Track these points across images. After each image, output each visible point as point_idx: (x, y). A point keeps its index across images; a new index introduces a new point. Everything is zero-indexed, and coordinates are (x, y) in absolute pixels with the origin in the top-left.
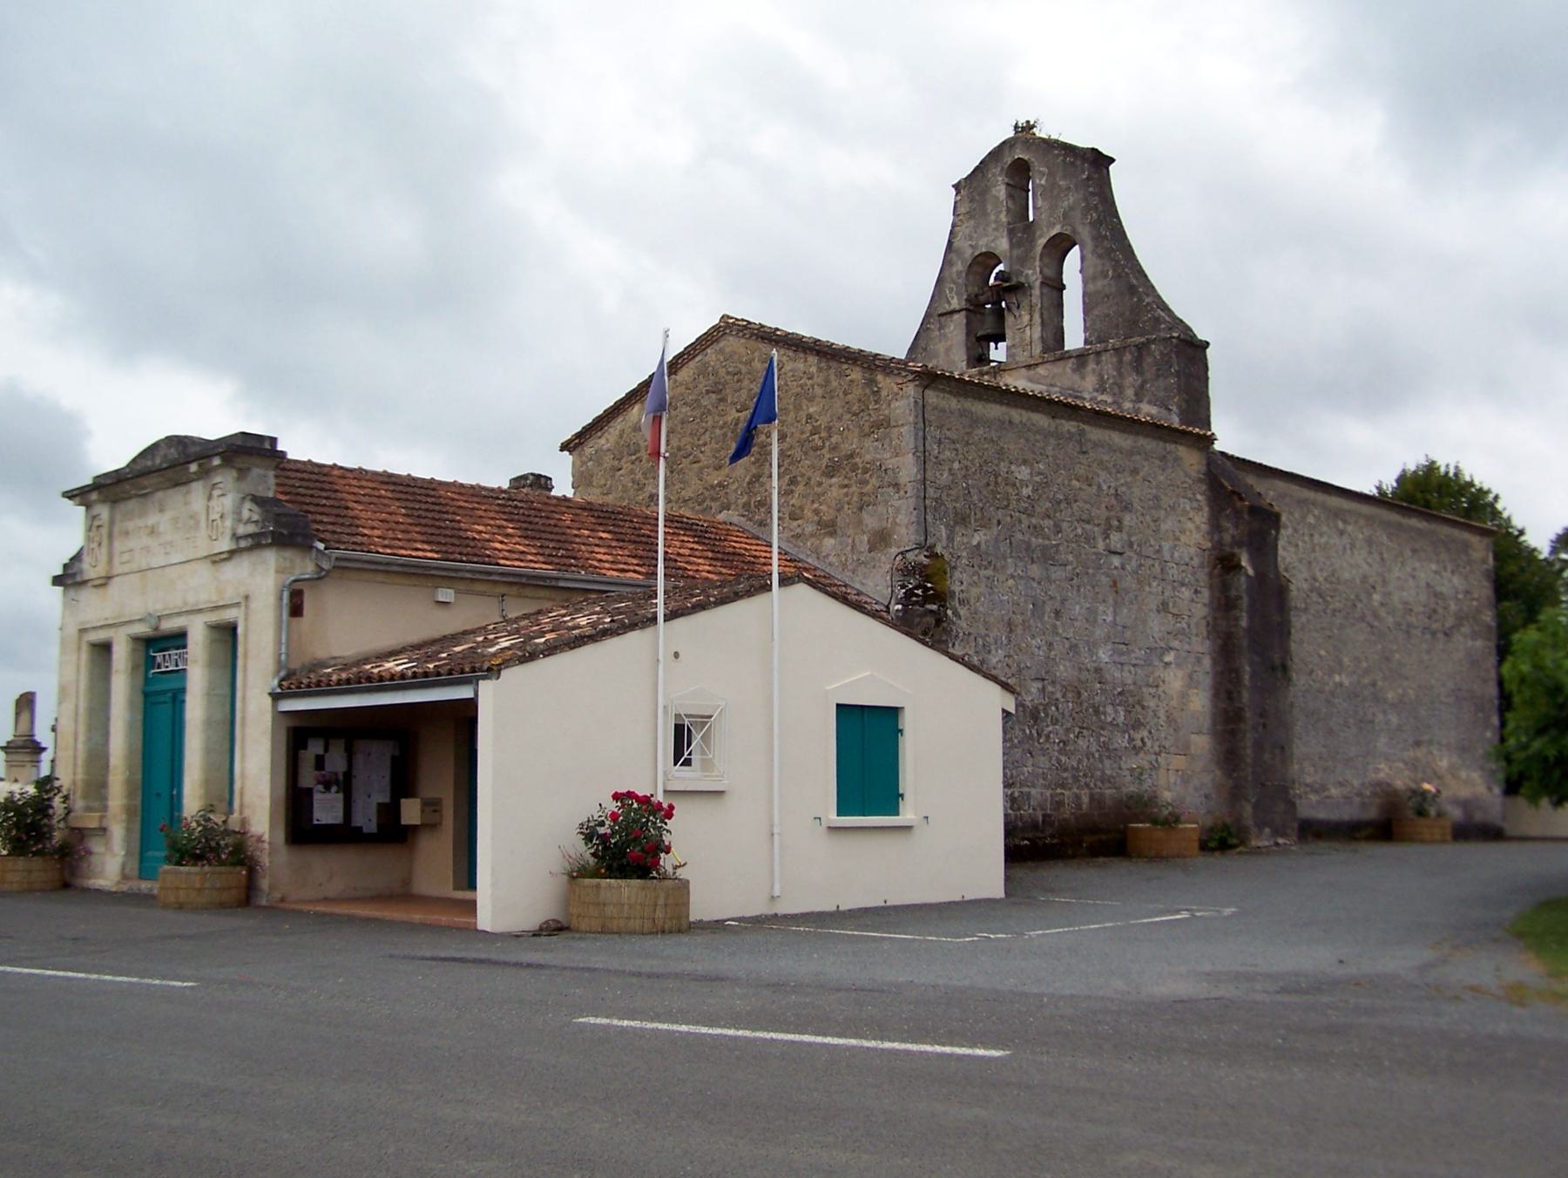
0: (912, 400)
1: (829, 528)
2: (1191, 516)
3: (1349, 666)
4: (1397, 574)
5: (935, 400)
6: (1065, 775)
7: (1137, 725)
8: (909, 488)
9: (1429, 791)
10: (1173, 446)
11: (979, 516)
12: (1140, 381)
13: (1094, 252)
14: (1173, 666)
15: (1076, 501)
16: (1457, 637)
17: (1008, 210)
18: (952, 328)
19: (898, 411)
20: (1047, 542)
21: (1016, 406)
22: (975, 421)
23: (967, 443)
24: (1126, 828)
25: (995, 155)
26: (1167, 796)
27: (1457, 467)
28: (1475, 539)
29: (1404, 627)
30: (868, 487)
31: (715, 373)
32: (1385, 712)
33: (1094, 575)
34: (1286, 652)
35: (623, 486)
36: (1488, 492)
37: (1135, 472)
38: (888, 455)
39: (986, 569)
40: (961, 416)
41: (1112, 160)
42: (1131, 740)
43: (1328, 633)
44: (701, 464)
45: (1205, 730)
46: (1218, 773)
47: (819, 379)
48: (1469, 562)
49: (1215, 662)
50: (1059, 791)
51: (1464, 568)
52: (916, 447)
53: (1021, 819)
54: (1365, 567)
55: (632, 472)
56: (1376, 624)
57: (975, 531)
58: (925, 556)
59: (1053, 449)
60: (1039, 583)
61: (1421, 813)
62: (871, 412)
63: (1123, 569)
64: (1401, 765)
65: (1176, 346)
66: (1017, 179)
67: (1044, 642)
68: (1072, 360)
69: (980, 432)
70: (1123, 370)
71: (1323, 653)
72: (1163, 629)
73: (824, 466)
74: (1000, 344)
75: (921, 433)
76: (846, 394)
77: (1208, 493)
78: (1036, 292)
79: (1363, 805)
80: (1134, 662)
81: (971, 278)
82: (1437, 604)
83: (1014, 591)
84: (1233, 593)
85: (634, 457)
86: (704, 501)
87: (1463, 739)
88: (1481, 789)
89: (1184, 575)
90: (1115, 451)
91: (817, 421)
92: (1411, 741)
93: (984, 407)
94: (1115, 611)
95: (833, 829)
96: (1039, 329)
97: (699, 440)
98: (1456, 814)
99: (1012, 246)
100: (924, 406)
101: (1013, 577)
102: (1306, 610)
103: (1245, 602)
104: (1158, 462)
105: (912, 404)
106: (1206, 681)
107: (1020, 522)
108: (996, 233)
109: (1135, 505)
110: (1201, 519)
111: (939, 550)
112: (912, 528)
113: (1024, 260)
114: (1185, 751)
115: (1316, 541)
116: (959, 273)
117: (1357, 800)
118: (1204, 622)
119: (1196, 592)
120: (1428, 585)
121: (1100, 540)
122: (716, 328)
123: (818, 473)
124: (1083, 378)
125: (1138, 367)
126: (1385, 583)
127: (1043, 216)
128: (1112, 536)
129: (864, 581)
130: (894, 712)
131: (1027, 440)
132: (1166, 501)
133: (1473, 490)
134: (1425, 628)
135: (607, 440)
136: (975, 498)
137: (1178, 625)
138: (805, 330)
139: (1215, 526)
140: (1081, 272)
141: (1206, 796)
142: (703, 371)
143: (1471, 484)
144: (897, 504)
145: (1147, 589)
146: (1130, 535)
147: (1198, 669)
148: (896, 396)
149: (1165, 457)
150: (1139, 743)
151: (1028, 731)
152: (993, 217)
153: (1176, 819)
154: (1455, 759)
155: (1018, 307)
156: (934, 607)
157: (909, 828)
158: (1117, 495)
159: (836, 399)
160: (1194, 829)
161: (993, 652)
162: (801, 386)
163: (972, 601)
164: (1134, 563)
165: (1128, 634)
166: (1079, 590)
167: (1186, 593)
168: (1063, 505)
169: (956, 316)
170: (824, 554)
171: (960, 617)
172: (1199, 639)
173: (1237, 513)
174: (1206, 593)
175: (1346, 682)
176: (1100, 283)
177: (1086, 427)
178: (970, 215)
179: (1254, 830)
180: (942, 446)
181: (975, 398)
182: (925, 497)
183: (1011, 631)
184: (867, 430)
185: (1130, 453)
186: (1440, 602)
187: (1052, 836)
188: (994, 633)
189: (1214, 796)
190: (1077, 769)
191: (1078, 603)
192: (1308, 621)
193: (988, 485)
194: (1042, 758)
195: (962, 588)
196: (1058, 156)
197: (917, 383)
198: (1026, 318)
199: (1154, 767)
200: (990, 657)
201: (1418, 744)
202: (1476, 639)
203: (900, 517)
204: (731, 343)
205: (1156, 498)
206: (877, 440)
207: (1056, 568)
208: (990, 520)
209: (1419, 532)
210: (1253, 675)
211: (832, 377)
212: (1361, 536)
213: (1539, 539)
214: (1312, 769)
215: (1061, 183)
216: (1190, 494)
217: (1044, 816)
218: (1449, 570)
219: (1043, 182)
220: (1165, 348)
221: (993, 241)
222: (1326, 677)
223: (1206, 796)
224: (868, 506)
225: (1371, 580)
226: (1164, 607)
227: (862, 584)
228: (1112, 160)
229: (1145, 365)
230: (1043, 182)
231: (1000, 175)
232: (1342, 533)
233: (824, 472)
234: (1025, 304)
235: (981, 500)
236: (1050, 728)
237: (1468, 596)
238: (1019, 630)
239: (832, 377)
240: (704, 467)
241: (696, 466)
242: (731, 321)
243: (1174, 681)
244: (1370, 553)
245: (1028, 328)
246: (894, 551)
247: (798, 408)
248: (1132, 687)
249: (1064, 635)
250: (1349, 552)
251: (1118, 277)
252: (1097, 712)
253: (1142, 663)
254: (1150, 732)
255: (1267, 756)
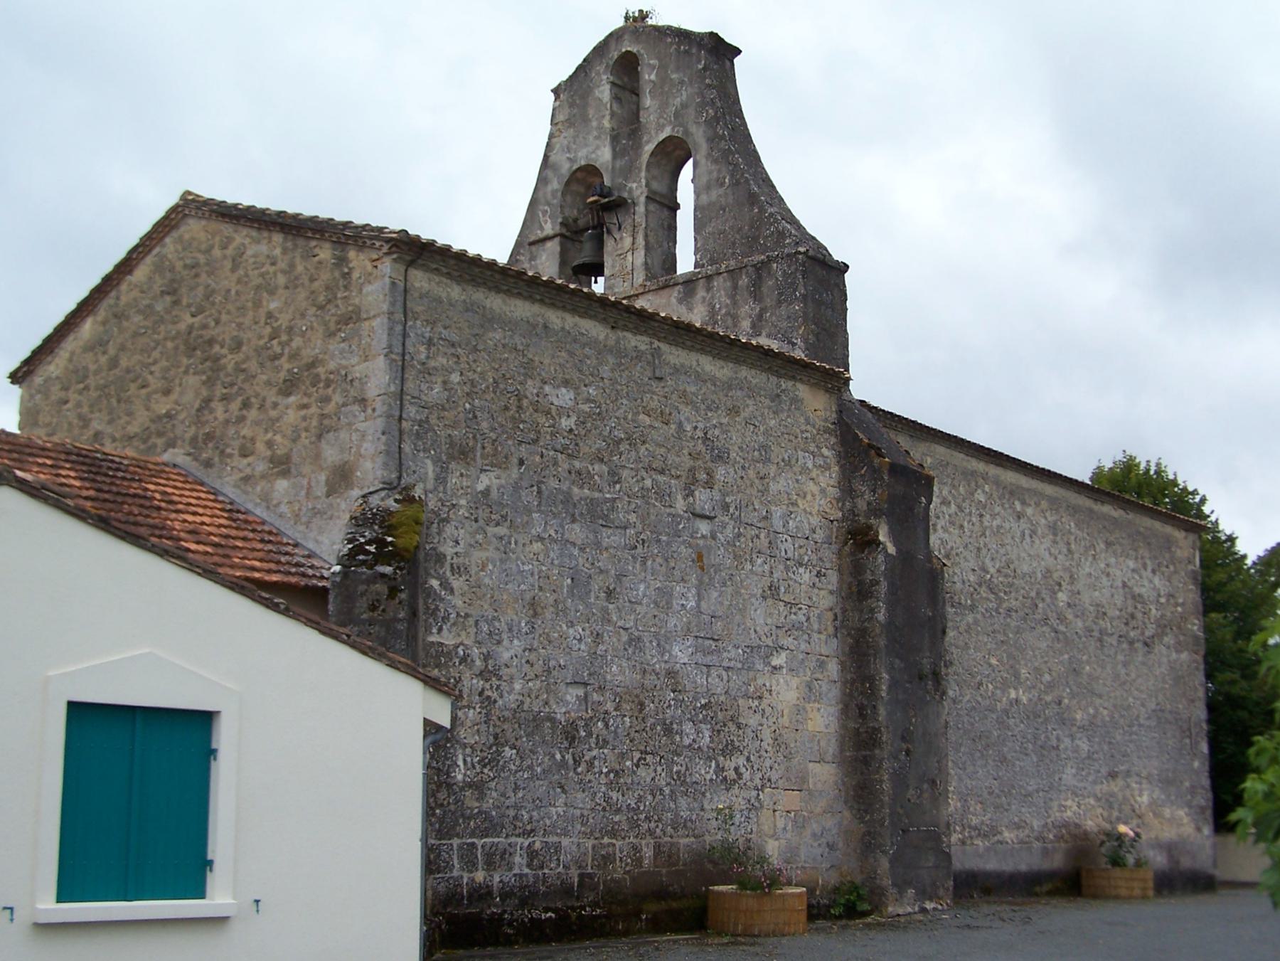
0: (387, 280)
1: (282, 466)
2: (814, 475)
3: (1027, 679)
4: (1087, 570)
5: (426, 285)
6: (617, 818)
7: (730, 749)
8: (378, 404)
9: (1126, 835)
10: (790, 383)
11: (489, 449)
12: (758, 309)
13: (708, 156)
14: (784, 670)
15: (644, 442)
16: (1159, 649)
17: (613, 115)
18: (544, 258)
19: (370, 298)
20: (596, 495)
21: (553, 305)
22: (490, 320)
23: (475, 349)
24: (706, 896)
25: (600, 50)
26: (773, 849)
27: (1158, 465)
28: (1179, 535)
29: (1096, 634)
30: (330, 406)
31: (172, 269)
32: (1072, 737)
33: (668, 543)
34: (939, 654)
36: (1195, 493)
37: (734, 411)
38: (355, 360)
39: (498, 524)
40: (467, 310)
41: (737, 51)
42: (720, 769)
43: (1001, 637)
44: (149, 389)
45: (829, 758)
46: (847, 814)
47: (282, 265)
48: (1173, 561)
49: (843, 667)
50: (606, 840)
51: (1167, 567)
52: (390, 346)
53: (544, 881)
54: (1051, 561)
55: (79, 405)
56: (1062, 628)
57: (482, 471)
58: (396, 501)
59: (612, 370)
60: (582, 550)
61: (1117, 862)
62: (339, 302)
63: (714, 537)
64: (1092, 801)
65: (803, 265)
66: (626, 79)
67: (588, 632)
68: (678, 288)
69: (498, 335)
70: (738, 297)
71: (994, 661)
72: (769, 621)
73: (281, 381)
74: (599, 279)
75: (399, 328)
76: (312, 280)
77: (838, 448)
78: (641, 209)
79: (1045, 852)
80: (725, 664)
81: (569, 198)
82: (1136, 608)
83: (541, 558)
84: (868, 576)
85: (81, 386)
86: (149, 438)
87: (1167, 770)
88: (1188, 829)
89: (802, 551)
90: (705, 381)
92: (1104, 771)
93: (504, 301)
94: (699, 594)
95: (47, 928)
96: (643, 253)
97: (149, 357)
98: (1159, 860)
99: (615, 156)
100: (406, 291)
101: (540, 538)
102: (973, 608)
103: (883, 587)
104: (767, 402)
105: (387, 287)
106: (831, 693)
107: (556, 464)
108: (598, 142)
109: (733, 455)
110: (828, 480)
111: (418, 492)
112: (380, 460)
113: (628, 172)
114: (800, 783)
115: (986, 524)
116: (554, 193)
117: (1037, 845)
118: (830, 615)
119: (819, 574)
120: (1125, 585)
121: (679, 497)
122: (174, 209)
123: (275, 390)
124: (690, 309)
125: (756, 296)
126: (1073, 579)
127: (652, 117)
128: (697, 493)
129: (320, 538)
130: (204, 720)
131: (571, 354)
132: (777, 453)
133: (1176, 489)
134: (1120, 636)
135: (57, 365)
136: (485, 425)
137: (793, 617)
138: (275, 205)
139: (847, 490)
140: (692, 181)
141: (831, 847)
142: (159, 268)
143: (1174, 483)
144: (362, 426)
145: (748, 566)
146: (724, 495)
147: (818, 676)
148: (369, 278)
149: (778, 396)
150: (731, 774)
151: (558, 757)
152: (594, 124)
153: (775, 880)
154: (1157, 794)
155: (620, 228)
156: (388, 570)
157: (223, 920)
158: (706, 439)
159: (299, 289)
160: (800, 895)
161: (506, 642)
162: (262, 275)
163: (473, 570)
164: (729, 532)
165: (719, 625)
166: (644, 563)
167: (805, 576)
168: (624, 447)
169: (549, 244)
170: (275, 502)
171: (452, 591)
172: (823, 637)
173: (875, 472)
174: (833, 578)
175: (1024, 699)
176: (714, 194)
177: (664, 347)
178: (570, 123)
179: (892, 891)
180: (433, 349)
181: (490, 289)
182: (401, 418)
183: (535, 615)
184: (332, 326)
185: (729, 386)
186: (1139, 606)
187: (595, 905)
188: (510, 615)
189: (841, 845)
190: (636, 810)
191: (644, 581)
192: (976, 622)
193: (506, 408)
194: (580, 795)
195: (458, 549)
196: (671, 44)
197: (395, 256)
198: (628, 241)
199: (754, 807)
200: (501, 649)
201: (1113, 775)
202: (1181, 652)
203: (365, 445)
204: (194, 228)
205: (765, 448)
206: (344, 340)
207: (610, 531)
208: (506, 457)
209: (1115, 522)
210: (893, 685)
211: (298, 260)
212: (1043, 521)
213: (1252, 547)
214: (979, 807)
215: (673, 76)
216: (812, 447)
217: (581, 876)
218: (1149, 569)
219: (653, 77)
220: (789, 266)
222: (998, 692)
223: (831, 847)
224: (328, 432)
225: (1056, 576)
226: (772, 592)
227: (317, 541)
228: (737, 51)
229: (765, 290)
230: (653, 77)
231: (605, 73)
232: (1019, 516)
233: (280, 389)
234: (627, 224)
235: (493, 429)
236: (595, 753)
237: (1172, 601)
238: (548, 615)
239: (298, 260)
241: (144, 391)
242: (190, 197)
243: (786, 691)
244: (1055, 542)
245: (630, 253)
246: (356, 493)
247: (257, 304)
248: (722, 698)
249: (620, 623)
250: (1028, 539)
251: (736, 184)
252: (668, 731)
253: (740, 666)
254: (748, 759)
255: (911, 793)
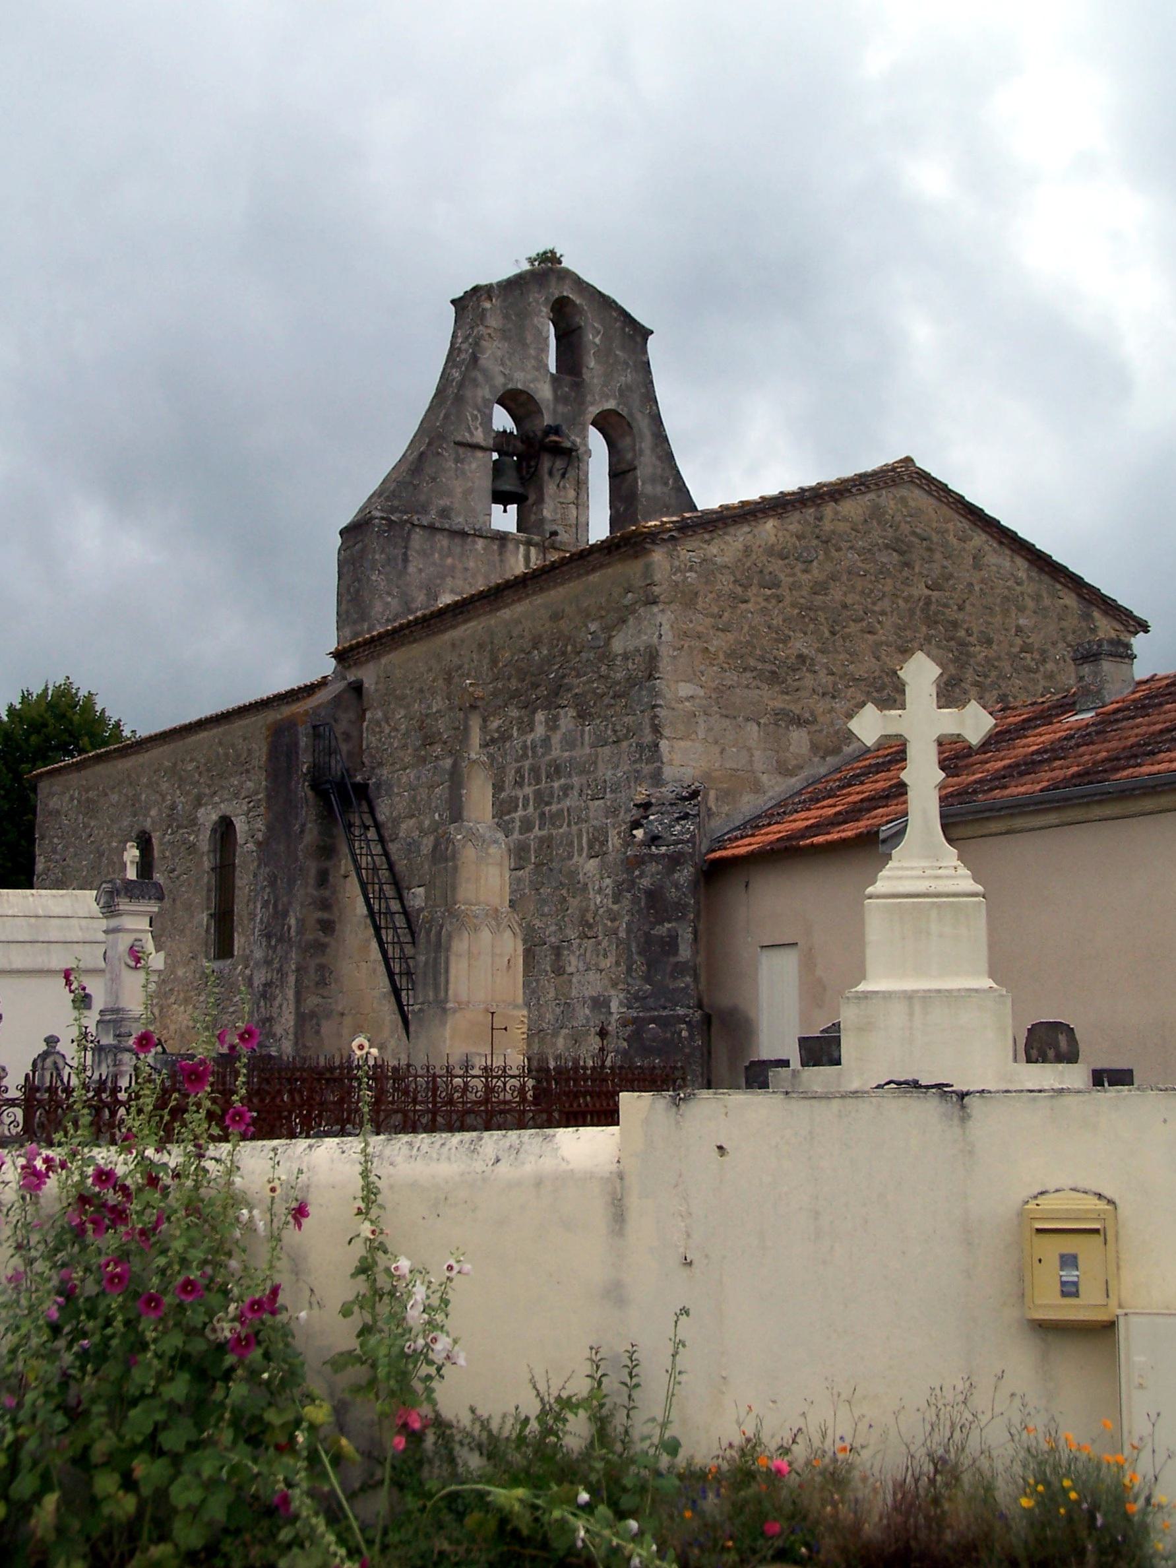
18: (474, 466)
35: (751, 628)
55: (764, 611)
74: (509, 507)
76: (1061, 619)
91: (1029, 637)
97: (874, 604)
142: (876, 513)
152: (532, 352)
162: (1008, 588)
219: (597, 340)
221: (533, 381)
240: (882, 643)
